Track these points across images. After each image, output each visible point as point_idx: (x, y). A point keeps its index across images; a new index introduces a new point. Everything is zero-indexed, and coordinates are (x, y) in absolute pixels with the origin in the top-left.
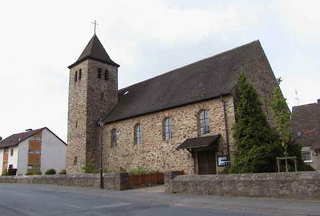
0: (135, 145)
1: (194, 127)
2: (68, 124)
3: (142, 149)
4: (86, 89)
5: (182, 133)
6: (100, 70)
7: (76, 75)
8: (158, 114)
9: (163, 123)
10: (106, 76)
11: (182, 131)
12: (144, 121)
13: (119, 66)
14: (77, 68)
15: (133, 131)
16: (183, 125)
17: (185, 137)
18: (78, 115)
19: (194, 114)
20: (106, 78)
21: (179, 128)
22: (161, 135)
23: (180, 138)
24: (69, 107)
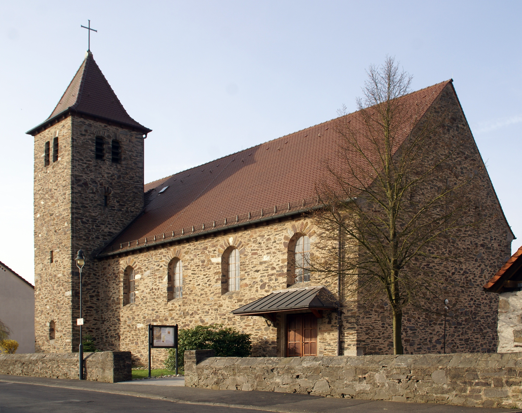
0: (169, 300)
1: (282, 267)
2: (36, 256)
3: (182, 308)
4: (69, 181)
5: (258, 279)
6: (100, 142)
7: (47, 150)
8: (215, 239)
9: (223, 258)
10: (114, 154)
11: (258, 275)
12: (186, 253)
13: (146, 131)
14: (49, 134)
15: (166, 272)
16: (261, 263)
17: (263, 287)
18: (54, 237)
19: (283, 241)
20: (116, 159)
21: (254, 269)
22: (220, 282)
23: (254, 289)
24: (36, 219)
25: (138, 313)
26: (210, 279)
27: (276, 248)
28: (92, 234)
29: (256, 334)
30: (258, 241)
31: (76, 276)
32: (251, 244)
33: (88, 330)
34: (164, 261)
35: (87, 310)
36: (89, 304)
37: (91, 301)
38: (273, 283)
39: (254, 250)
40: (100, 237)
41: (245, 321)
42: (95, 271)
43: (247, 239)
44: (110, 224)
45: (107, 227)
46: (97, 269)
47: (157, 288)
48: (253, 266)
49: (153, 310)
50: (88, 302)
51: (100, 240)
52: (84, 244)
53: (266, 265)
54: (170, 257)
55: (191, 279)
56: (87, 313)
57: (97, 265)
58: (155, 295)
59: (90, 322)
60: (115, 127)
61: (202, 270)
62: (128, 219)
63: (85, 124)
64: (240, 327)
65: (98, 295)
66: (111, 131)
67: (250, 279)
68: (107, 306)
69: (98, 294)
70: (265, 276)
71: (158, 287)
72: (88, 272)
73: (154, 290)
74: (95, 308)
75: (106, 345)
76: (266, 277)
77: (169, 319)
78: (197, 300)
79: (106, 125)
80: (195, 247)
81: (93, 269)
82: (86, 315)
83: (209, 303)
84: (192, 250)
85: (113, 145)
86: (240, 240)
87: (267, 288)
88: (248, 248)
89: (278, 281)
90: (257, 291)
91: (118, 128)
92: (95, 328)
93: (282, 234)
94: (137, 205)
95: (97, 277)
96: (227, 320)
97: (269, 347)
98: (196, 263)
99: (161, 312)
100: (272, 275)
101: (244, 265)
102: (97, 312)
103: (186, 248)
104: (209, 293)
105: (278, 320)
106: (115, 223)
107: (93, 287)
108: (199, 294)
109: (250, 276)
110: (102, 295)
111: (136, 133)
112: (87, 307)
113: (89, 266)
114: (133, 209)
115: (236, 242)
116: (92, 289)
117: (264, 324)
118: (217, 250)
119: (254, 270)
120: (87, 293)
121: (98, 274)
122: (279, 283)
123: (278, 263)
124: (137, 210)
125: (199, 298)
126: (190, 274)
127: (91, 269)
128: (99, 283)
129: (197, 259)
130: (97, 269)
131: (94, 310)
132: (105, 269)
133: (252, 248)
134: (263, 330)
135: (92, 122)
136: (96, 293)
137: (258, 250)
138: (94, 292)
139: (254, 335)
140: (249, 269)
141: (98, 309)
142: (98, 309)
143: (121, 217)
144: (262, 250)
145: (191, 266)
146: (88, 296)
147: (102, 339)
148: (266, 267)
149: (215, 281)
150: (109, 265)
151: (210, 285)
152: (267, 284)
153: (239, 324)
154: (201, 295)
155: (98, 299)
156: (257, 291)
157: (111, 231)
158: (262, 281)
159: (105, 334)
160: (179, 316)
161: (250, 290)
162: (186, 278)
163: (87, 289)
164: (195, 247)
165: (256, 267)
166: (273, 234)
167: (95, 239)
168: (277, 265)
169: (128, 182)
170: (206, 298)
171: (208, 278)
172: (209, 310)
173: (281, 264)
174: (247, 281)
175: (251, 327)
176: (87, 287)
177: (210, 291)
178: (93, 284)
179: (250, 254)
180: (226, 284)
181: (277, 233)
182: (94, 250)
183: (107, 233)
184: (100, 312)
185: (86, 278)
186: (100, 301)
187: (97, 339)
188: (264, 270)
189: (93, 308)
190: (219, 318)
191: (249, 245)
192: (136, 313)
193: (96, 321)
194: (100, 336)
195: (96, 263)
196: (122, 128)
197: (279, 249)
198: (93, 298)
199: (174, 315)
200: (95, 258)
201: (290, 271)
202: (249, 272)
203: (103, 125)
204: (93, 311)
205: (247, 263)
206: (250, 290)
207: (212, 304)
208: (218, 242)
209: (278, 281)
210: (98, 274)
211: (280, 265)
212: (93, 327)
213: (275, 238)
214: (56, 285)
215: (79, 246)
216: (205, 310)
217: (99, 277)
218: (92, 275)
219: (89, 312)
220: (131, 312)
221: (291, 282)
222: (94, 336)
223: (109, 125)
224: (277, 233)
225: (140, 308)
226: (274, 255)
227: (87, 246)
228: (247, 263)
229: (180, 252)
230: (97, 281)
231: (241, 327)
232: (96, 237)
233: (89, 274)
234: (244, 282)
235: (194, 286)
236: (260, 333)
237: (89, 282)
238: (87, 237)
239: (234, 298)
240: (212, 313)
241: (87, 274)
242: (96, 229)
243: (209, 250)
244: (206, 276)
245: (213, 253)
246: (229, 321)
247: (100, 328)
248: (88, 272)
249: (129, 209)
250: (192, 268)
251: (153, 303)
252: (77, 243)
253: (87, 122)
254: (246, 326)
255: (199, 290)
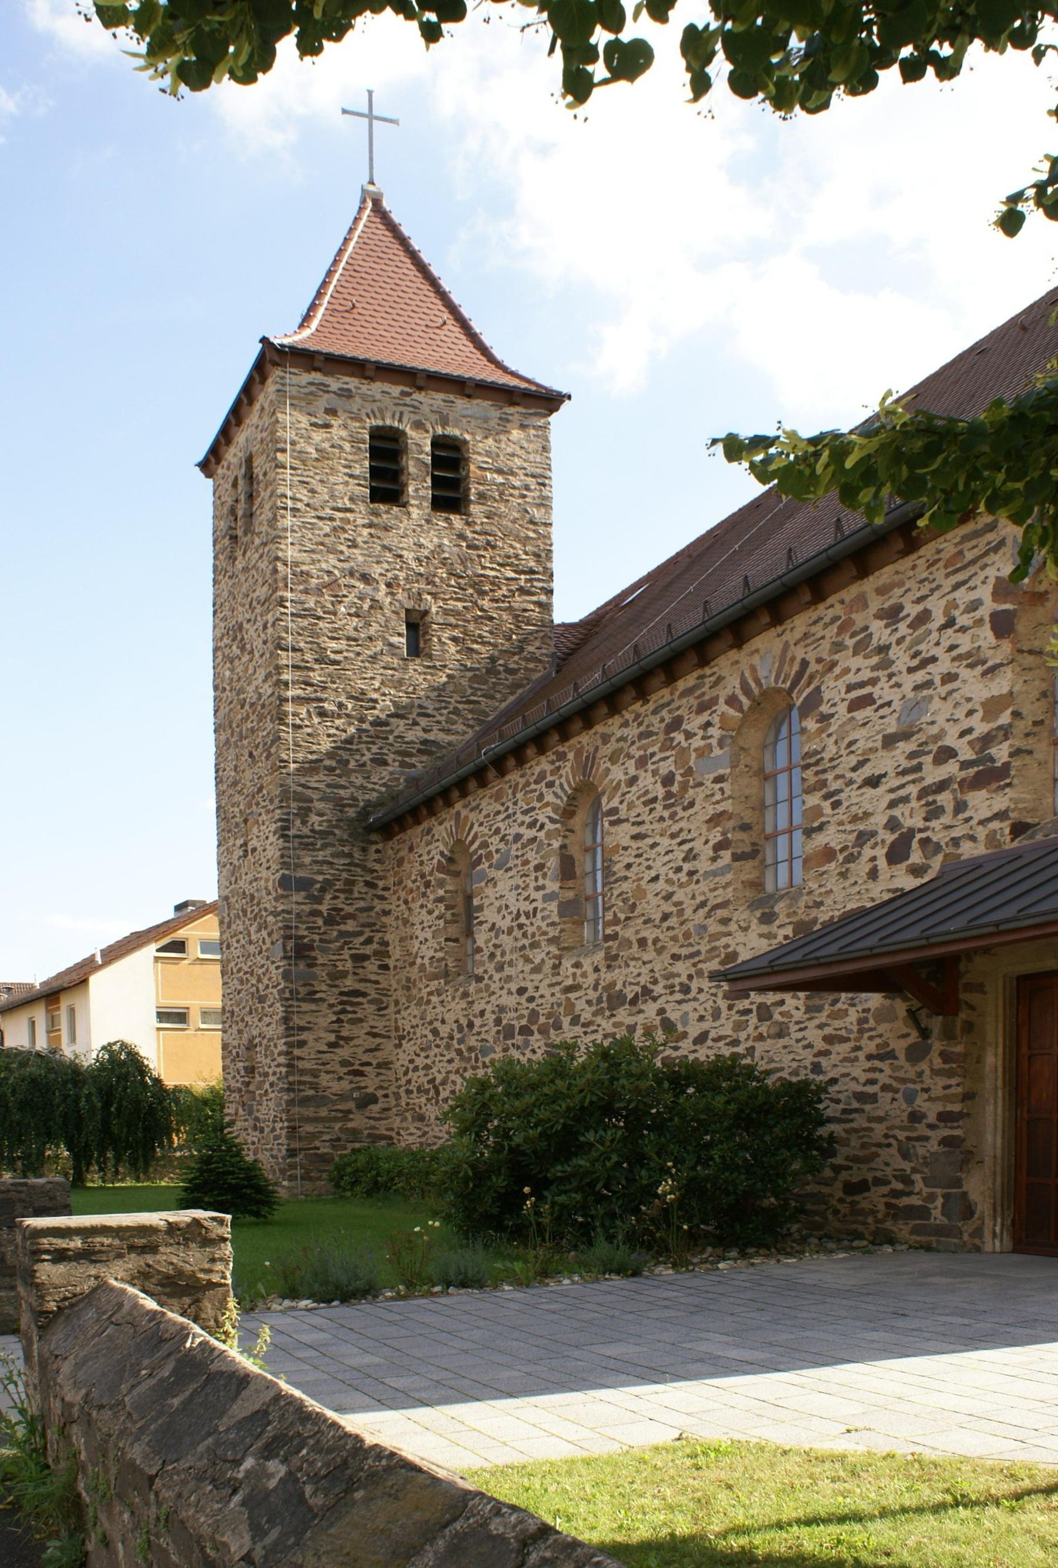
3: (606, 977)
5: (879, 820)
11: (876, 800)
21: (860, 776)
23: (862, 868)
25: (483, 1006)
26: (691, 850)
27: (954, 653)
28: (358, 750)
29: (871, 1075)
30: (874, 642)
31: (298, 890)
32: (848, 660)
33: (345, 1070)
34: (547, 804)
35: (341, 1003)
36: (349, 983)
37: (355, 974)
38: (948, 827)
39: (862, 685)
40: (390, 758)
41: (823, 1020)
42: (372, 871)
43: (826, 645)
44: (428, 716)
45: (415, 723)
46: (377, 867)
47: (530, 908)
48: (853, 760)
49: (521, 991)
50: (345, 977)
51: (390, 769)
52: (328, 786)
53: (910, 746)
54: (566, 787)
55: (631, 860)
56: (344, 1011)
57: (378, 851)
58: (525, 935)
59: (355, 1042)
60: (441, 396)
61: (666, 814)
62: (498, 696)
63: (328, 392)
64: (805, 1047)
65: (383, 953)
66: (426, 409)
67: (841, 823)
68: (408, 989)
69: (383, 948)
70: (905, 800)
71: (535, 905)
72: (345, 875)
73: (523, 920)
74: (373, 995)
75: (406, 1119)
76: (914, 804)
77: (566, 1021)
78: (650, 942)
79: (407, 389)
80: (642, 729)
81: (364, 868)
82: (339, 1021)
83: (692, 950)
84: (633, 743)
85: (434, 457)
86: (799, 653)
87: (916, 857)
88: (832, 684)
89: (966, 815)
90: (873, 874)
91: (452, 397)
92: (374, 1062)
93: (982, 575)
94: (531, 649)
95: (381, 893)
96: (753, 1019)
97: (927, 1139)
98: (646, 792)
99: (542, 996)
100: (942, 786)
101: (817, 763)
102: (379, 1009)
103: (613, 739)
104: (689, 906)
105: (972, 1008)
106: (445, 712)
107: (363, 925)
108: (657, 916)
109: (841, 810)
110: (396, 952)
111: (524, 411)
112: (342, 994)
113: (350, 855)
114: (516, 663)
115: (786, 667)
116: (361, 933)
117: (905, 1030)
118: (716, 720)
119: (860, 781)
120: (342, 948)
121: (381, 884)
122: (973, 822)
123: (965, 724)
124: (531, 665)
125: (657, 933)
126: (626, 841)
127: (357, 865)
128: (386, 913)
129: (650, 774)
130: (377, 867)
131: (370, 1002)
132: (400, 862)
133: (851, 678)
134: (902, 1056)
135: (352, 383)
136: (375, 946)
137: (873, 682)
138: (369, 941)
139: (862, 1080)
140: (837, 777)
141: (384, 999)
142: (384, 999)
143: (469, 691)
144: (890, 676)
145: (631, 806)
146: (347, 957)
147: (397, 1096)
148: (912, 755)
149: (711, 853)
150: (411, 849)
151: (691, 873)
152: (919, 836)
153: (800, 1035)
154: (665, 917)
155: (385, 967)
156: (873, 874)
157: (431, 737)
158: (893, 824)
159: (403, 1081)
160: (594, 1008)
161: (843, 875)
162: (616, 858)
163: (342, 934)
164: (642, 729)
165: (869, 765)
166: (939, 587)
167: (368, 768)
168: (962, 734)
169: (492, 573)
170: (679, 932)
171: (686, 847)
172: (690, 977)
173: (981, 728)
174: (831, 837)
175: (846, 1047)
176: (342, 927)
177: (693, 897)
178: (363, 918)
179: (842, 708)
180: (756, 862)
181: (960, 577)
182: (368, 803)
183: (417, 746)
184: (392, 1008)
185: (335, 898)
186: (392, 972)
187: (381, 1100)
188: (904, 773)
189: (364, 995)
190: (725, 1013)
191: (837, 670)
192: (477, 1008)
193: (378, 1040)
194: (393, 1089)
195: (374, 848)
196: (469, 396)
197: (969, 655)
198: (366, 964)
199: (581, 1005)
200: (370, 829)
201: (1030, 752)
202: (841, 791)
203: (396, 390)
204: (366, 1006)
205: (831, 750)
206: (843, 875)
207: (698, 953)
208: (721, 686)
209: (966, 815)
210: (381, 884)
211: (975, 734)
212: (366, 1058)
213: (953, 605)
214: (253, 929)
215: (308, 792)
216: (677, 981)
217: (386, 894)
218: (359, 888)
219: (349, 1008)
220: (464, 1006)
221: (1033, 810)
222: (370, 1090)
223: (420, 389)
224: (960, 577)
225: (488, 986)
226: (949, 687)
227: (342, 792)
228: (831, 750)
229: (594, 758)
230: (379, 906)
231: (810, 1046)
232: (372, 760)
233: (350, 883)
234: (820, 840)
235: (638, 886)
236: (888, 1071)
237: (349, 909)
238: (338, 762)
239: (782, 919)
240: (701, 990)
241: (339, 885)
242: (372, 733)
243: (688, 727)
244: (679, 840)
245: (704, 738)
246: (760, 1020)
247: (391, 1063)
248: (345, 875)
249: (501, 662)
250: (633, 813)
251: (520, 968)
252: (303, 781)
253: (334, 383)
254: (829, 1039)
255: (655, 901)
